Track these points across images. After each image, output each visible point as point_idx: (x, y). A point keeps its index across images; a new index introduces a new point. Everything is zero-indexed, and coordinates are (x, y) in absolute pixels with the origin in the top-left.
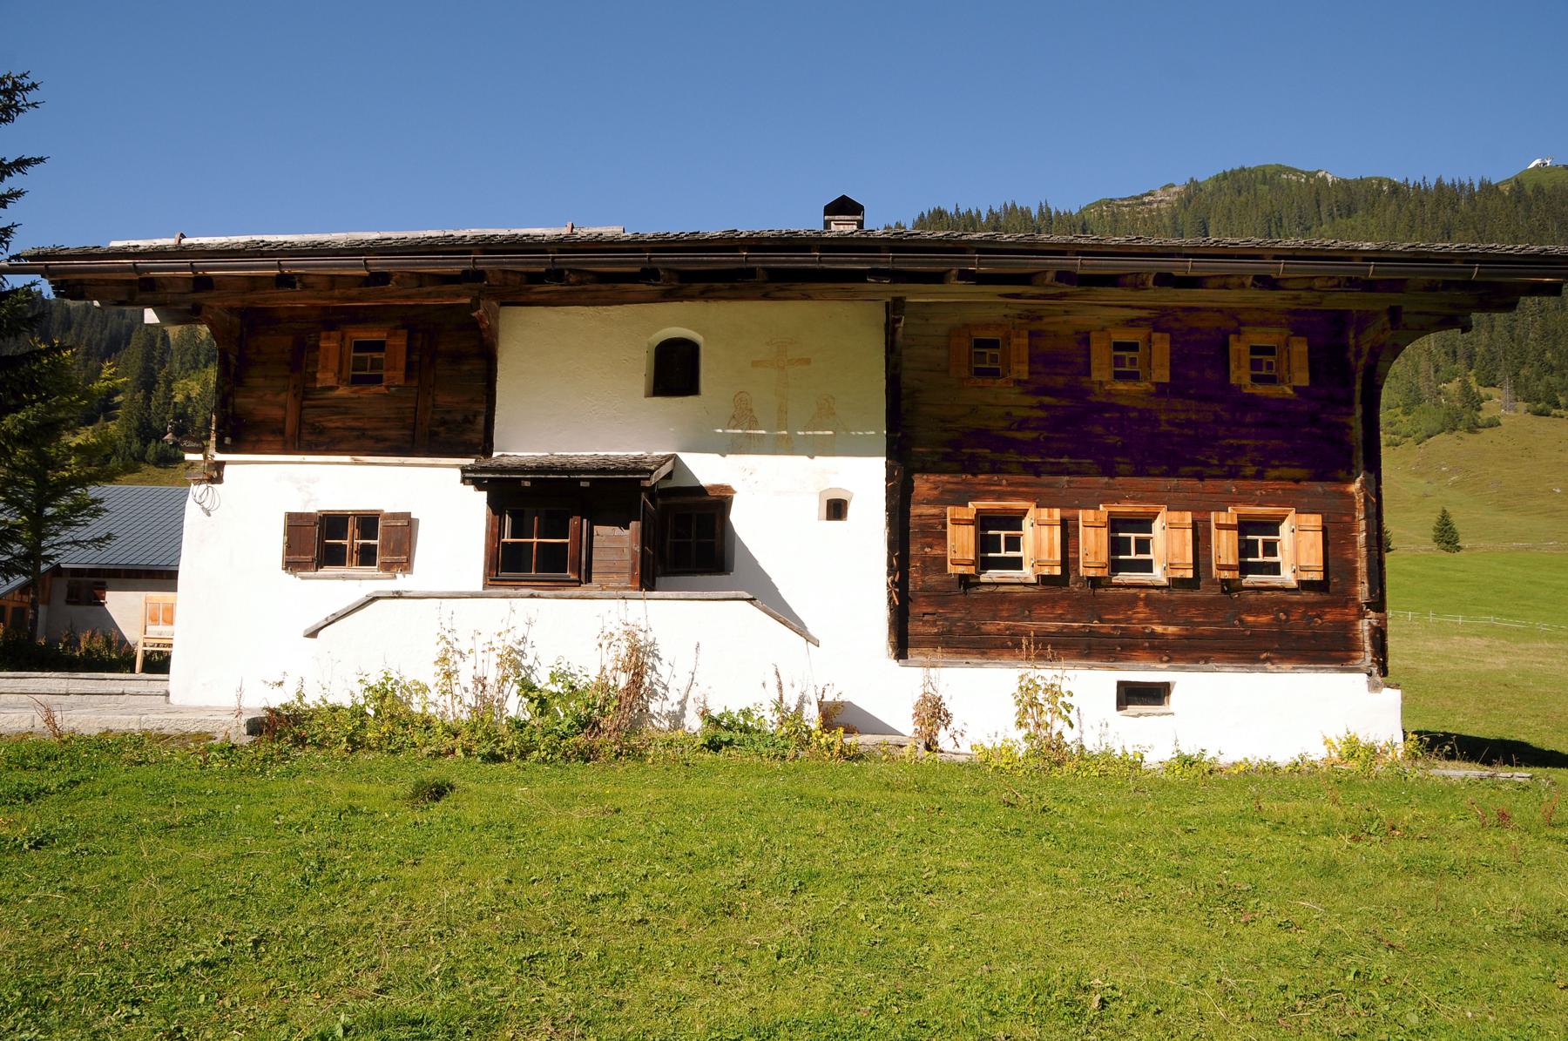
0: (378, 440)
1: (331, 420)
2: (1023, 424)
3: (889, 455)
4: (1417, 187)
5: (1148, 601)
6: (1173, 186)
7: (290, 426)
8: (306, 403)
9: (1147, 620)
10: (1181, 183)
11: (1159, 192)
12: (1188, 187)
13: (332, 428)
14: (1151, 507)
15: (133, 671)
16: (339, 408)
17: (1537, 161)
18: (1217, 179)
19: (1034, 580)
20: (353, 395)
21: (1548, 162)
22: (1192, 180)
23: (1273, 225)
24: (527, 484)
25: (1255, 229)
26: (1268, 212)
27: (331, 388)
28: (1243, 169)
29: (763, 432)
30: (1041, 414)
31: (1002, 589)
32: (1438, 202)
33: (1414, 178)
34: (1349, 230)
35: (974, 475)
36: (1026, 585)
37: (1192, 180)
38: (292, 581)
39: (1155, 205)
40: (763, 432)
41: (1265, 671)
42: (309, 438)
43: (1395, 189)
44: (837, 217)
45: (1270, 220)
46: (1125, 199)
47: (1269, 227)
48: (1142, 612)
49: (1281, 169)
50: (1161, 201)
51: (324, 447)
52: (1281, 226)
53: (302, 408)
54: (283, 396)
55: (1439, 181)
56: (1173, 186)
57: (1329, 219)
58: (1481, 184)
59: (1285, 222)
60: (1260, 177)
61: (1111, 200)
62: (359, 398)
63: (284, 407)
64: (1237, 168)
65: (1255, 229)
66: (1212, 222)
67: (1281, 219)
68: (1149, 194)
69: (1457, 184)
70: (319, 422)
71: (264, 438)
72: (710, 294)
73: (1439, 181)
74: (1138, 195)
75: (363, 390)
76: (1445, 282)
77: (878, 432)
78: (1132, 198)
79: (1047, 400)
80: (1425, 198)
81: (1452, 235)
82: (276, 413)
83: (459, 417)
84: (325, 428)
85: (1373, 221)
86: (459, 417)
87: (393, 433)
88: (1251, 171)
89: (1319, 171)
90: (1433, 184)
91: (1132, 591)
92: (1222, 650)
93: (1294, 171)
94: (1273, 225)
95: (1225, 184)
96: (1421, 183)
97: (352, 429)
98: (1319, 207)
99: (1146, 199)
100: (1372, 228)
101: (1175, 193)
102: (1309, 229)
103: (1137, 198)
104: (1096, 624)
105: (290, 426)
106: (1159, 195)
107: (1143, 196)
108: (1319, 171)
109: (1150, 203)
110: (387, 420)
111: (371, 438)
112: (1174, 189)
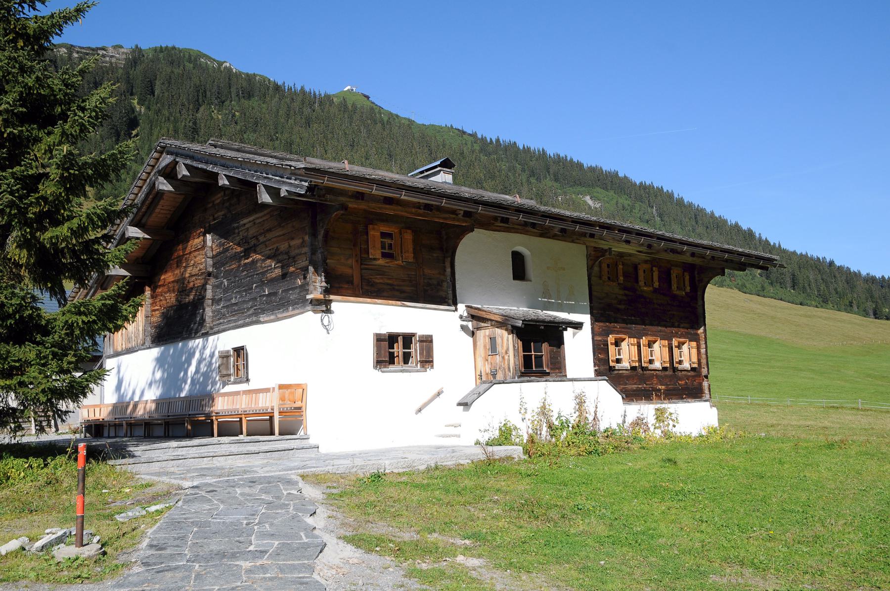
0: (402, 292)
1: (376, 278)
2: (620, 302)
3: (592, 314)
4: (290, 89)
5: (657, 376)
6: (121, 47)
7: (356, 280)
8: (363, 266)
9: (657, 384)
10: (128, 45)
11: (111, 50)
12: (133, 51)
13: (377, 283)
14: (623, 336)
15: (212, 436)
16: (380, 271)
17: (349, 87)
18: (155, 50)
19: (629, 368)
20: (386, 265)
21: (354, 89)
22: (137, 47)
23: (200, 94)
24: (543, 327)
25: (189, 95)
26: (197, 85)
27: (375, 259)
28: (174, 48)
29: (553, 301)
30: (625, 298)
31: (621, 372)
32: (303, 102)
33: (289, 83)
34: (251, 109)
35: (610, 323)
36: (626, 370)
37: (137, 47)
38: (377, 373)
39: (108, 59)
40: (553, 301)
41: (688, 402)
42: (366, 288)
43: (277, 88)
44: (444, 169)
45: (199, 91)
46: (83, 48)
47: (198, 96)
48: (655, 381)
49: (201, 55)
50: (112, 56)
51: (375, 294)
52: (205, 96)
53: (361, 269)
54: (349, 262)
55: (302, 88)
56: (121, 47)
57: (237, 99)
58: (325, 96)
59: (208, 93)
60: (187, 56)
61: (72, 46)
62: (389, 266)
63: (351, 267)
64: (170, 45)
65: (189, 95)
66: (158, 83)
67: (205, 92)
68: (103, 49)
69: (312, 92)
70: (371, 278)
71: (343, 286)
72: (556, 238)
73: (302, 88)
74: (94, 47)
75: (391, 262)
76: (749, 264)
77: (586, 303)
78: (89, 48)
79: (627, 292)
80: (295, 97)
81: (311, 126)
82: (348, 271)
83: (435, 282)
84: (374, 282)
85: (264, 106)
86: (435, 282)
87: (408, 289)
88: (180, 51)
89: (225, 62)
90: (299, 89)
91: (653, 372)
92: (675, 395)
93: (209, 58)
94: (200, 94)
95: (161, 55)
96: (293, 87)
97: (388, 284)
98: (230, 88)
99: (101, 52)
100: (264, 110)
101: (123, 53)
102: (223, 102)
103: (93, 50)
104: (645, 385)
105: (356, 280)
106: (111, 52)
107: (98, 49)
108: (225, 62)
109: (104, 56)
110: (404, 281)
111: (398, 290)
112: (122, 50)
